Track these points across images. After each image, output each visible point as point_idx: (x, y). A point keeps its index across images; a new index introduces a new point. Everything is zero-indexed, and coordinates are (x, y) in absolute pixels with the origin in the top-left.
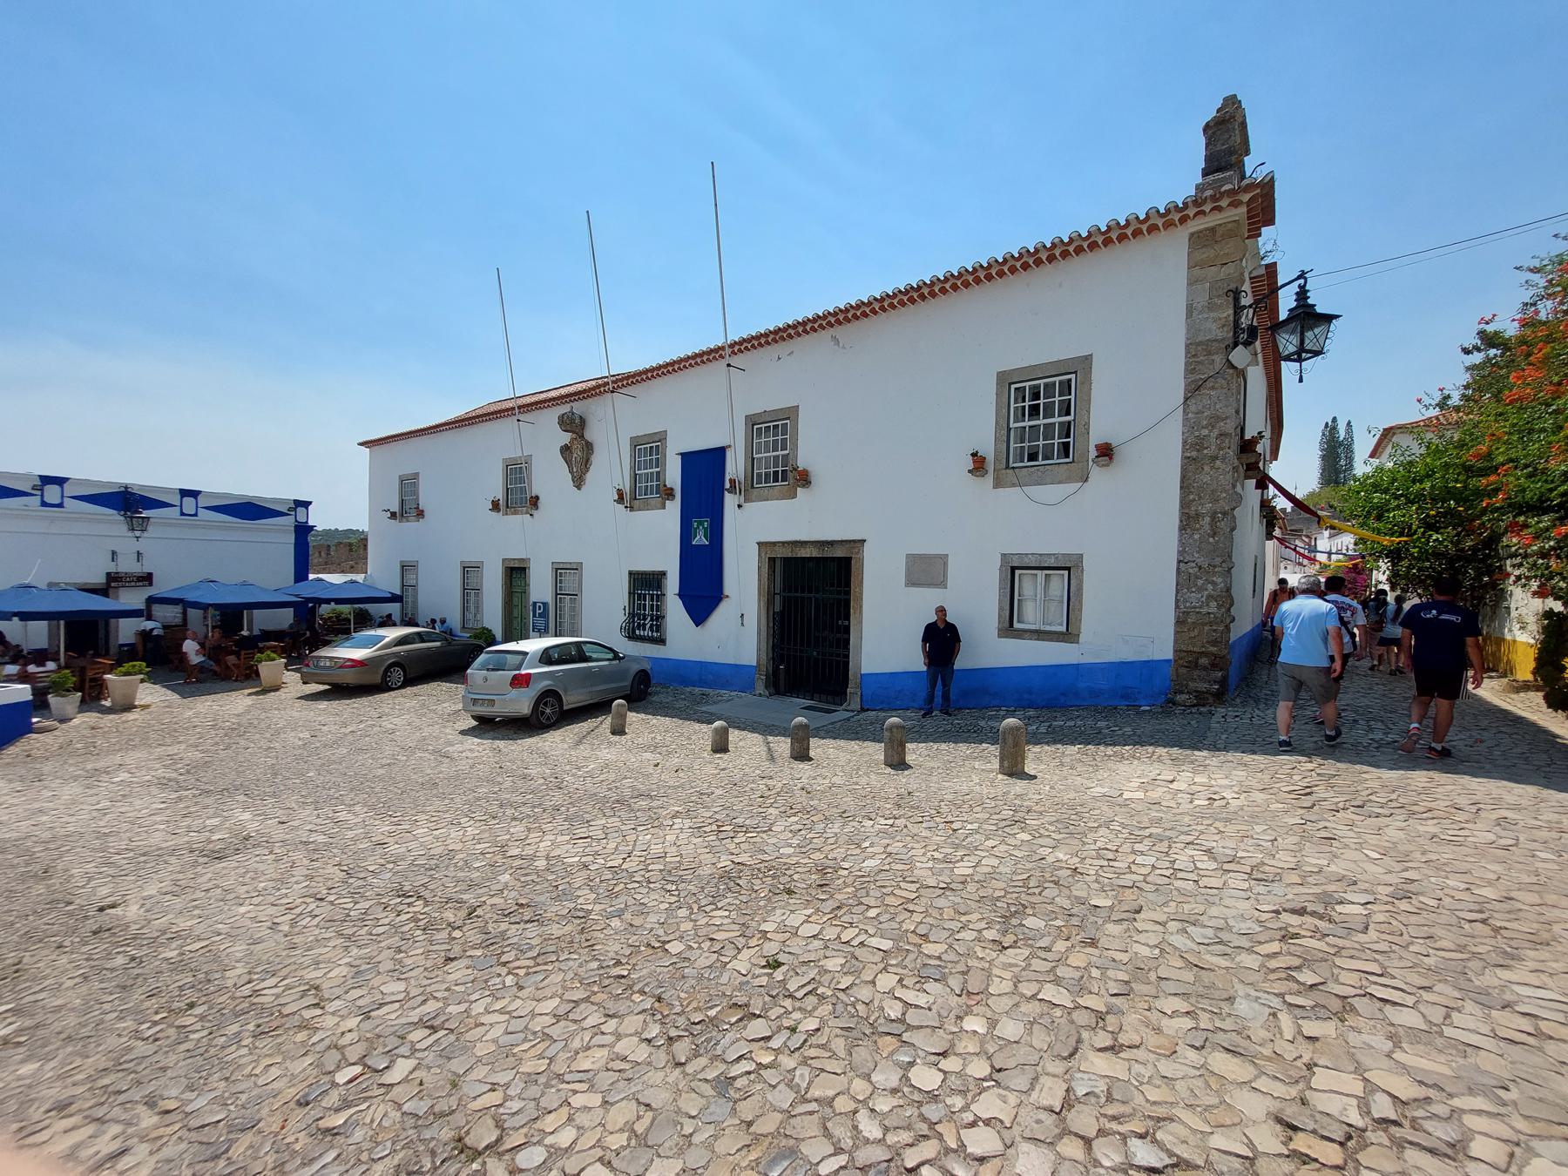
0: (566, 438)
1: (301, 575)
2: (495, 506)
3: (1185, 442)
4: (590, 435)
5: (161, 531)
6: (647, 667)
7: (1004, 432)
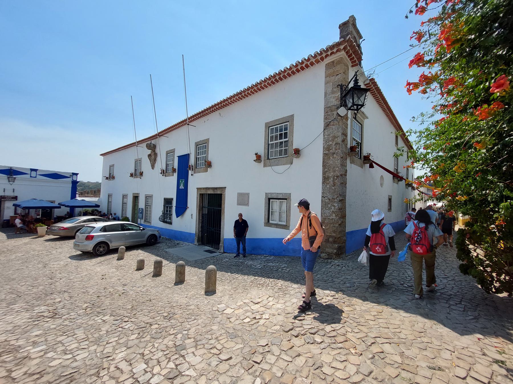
0: (149, 152)
1: (73, 196)
2: (132, 175)
3: (324, 147)
4: (157, 151)
5: (19, 183)
6: (156, 233)
7: (268, 146)
